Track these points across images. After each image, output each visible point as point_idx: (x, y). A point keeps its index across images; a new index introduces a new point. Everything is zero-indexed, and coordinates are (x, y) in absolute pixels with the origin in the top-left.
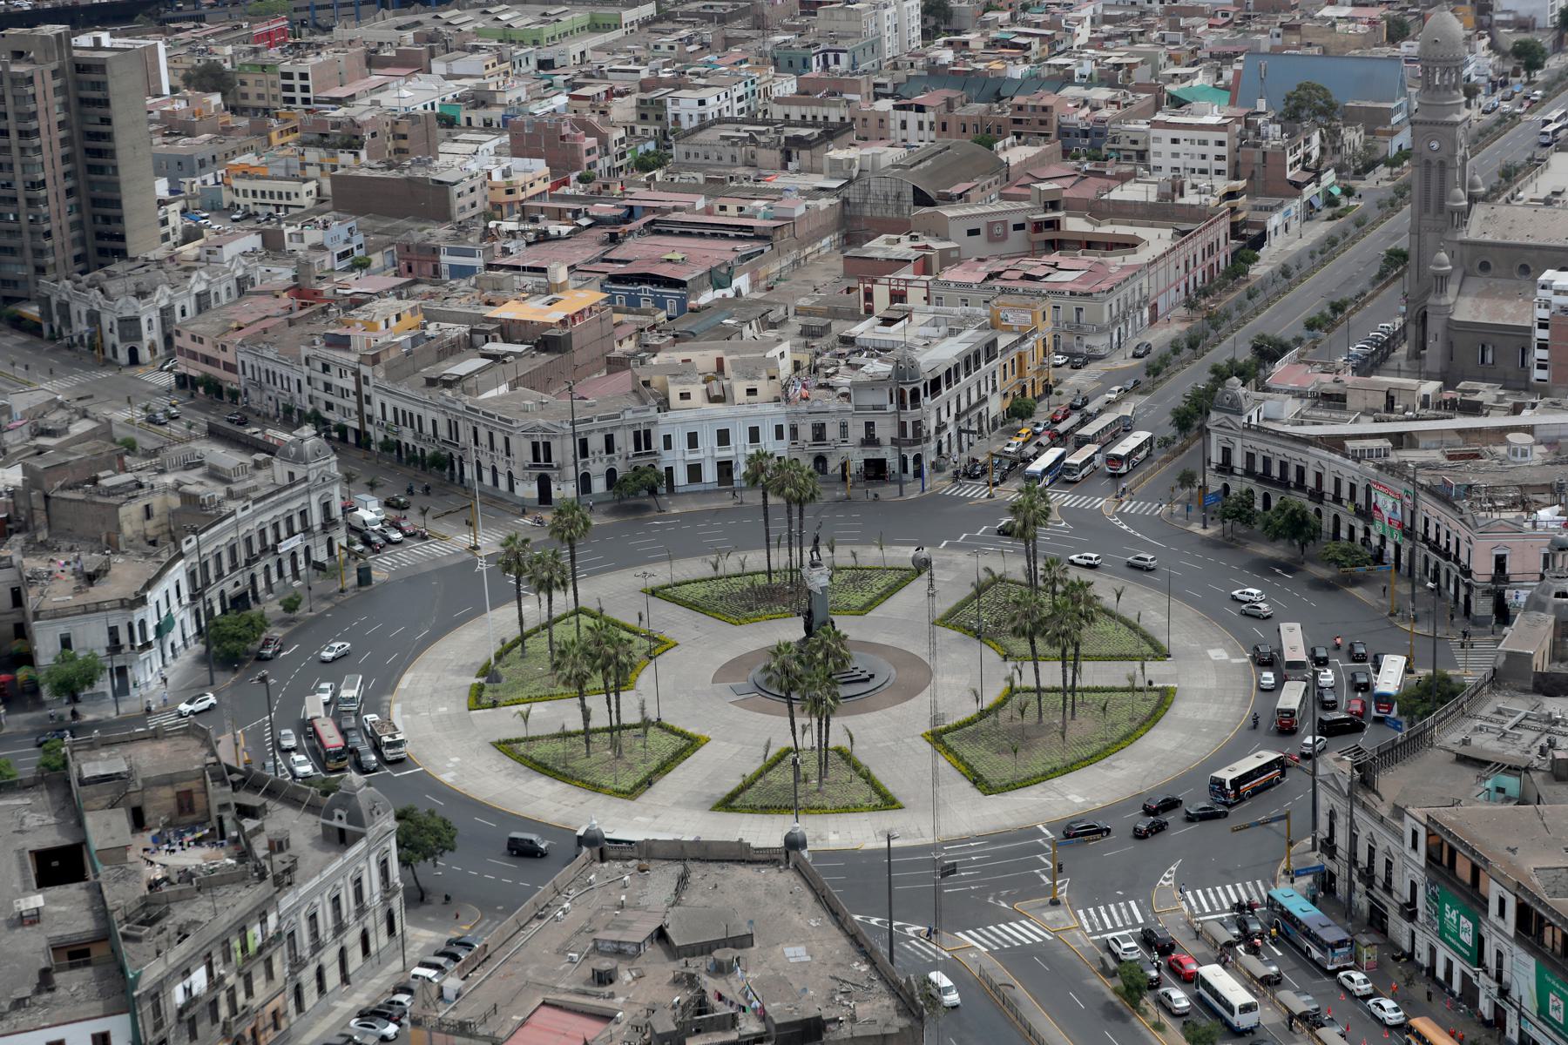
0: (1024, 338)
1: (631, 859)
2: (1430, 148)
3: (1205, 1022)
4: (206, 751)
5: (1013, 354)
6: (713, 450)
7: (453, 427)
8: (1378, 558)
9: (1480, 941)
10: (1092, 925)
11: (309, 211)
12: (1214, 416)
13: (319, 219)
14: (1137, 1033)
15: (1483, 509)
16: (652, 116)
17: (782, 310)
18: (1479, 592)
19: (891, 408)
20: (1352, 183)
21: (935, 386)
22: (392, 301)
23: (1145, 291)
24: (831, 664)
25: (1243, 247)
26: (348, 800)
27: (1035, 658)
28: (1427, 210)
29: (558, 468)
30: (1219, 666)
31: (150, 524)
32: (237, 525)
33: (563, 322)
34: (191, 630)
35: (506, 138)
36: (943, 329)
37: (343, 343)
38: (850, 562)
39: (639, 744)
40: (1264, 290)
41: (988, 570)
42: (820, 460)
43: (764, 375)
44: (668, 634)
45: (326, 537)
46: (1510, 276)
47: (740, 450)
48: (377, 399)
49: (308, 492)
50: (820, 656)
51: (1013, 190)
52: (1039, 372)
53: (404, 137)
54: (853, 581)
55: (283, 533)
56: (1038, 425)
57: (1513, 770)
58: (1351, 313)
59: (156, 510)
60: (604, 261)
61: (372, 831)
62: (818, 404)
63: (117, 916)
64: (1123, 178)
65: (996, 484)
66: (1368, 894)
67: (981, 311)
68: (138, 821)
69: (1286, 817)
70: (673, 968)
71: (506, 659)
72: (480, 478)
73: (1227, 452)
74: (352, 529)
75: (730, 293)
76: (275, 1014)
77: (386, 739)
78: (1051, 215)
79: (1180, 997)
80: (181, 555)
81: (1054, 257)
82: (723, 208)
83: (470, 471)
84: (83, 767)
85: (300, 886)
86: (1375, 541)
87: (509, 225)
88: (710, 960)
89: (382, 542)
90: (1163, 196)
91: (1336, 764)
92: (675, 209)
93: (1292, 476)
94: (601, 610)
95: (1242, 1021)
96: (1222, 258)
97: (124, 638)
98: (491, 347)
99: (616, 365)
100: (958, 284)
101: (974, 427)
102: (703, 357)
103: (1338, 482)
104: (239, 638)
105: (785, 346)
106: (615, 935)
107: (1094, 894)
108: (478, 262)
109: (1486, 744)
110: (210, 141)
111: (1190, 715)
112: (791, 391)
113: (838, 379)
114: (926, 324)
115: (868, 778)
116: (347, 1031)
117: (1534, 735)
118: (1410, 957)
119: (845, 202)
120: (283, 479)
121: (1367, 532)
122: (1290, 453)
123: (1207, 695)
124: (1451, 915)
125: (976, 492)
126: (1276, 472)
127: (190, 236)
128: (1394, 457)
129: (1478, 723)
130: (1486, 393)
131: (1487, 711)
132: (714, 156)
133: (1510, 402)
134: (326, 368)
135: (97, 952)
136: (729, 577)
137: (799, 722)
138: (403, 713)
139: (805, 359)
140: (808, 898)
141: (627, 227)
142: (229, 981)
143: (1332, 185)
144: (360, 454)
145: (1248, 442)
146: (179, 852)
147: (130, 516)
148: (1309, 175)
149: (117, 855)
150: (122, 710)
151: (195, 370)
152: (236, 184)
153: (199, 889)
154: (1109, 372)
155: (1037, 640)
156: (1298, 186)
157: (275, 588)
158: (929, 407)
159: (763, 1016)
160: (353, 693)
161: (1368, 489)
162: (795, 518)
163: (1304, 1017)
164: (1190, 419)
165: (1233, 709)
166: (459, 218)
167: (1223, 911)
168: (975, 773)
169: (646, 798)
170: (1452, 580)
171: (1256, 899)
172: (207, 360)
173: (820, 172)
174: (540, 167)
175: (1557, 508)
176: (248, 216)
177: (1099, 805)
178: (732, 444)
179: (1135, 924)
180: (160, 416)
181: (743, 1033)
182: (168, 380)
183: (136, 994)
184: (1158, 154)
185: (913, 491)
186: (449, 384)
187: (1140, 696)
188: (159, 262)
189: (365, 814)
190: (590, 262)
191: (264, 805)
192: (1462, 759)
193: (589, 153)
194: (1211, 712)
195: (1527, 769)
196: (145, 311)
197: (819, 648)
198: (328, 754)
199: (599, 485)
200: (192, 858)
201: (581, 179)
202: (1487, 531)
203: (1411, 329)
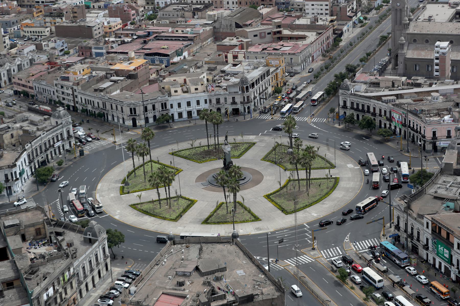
0: (277, 69)
1: (183, 244)
2: (397, 5)
3: (366, 286)
4: (43, 215)
5: (274, 74)
6: (186, 108)
7: (104, 104)
8: (394, 133)
9: (451, 256)
10: (326, 256)
11: (48, 37)
12: (340, 91)
13: (52, 39)
14: (346, 291)
15: (427, 117)
16: (150, 3)
17: (201, 63)
18: (428, 143)
19: (240, 92)
20: (366, 15)
21: (253, 85)
22: (79, 65)
23: (310, 52)
24: (237, 176)
25: (337, 37)
26: (91, 229)
27: (297, 169)
28: (396, 24)
29: (138, 116)
30: (351, 169)
31: (13, 140)
32: (41, 139)
33: (134, 70)
34: (29, 173)
35: (107, 11)
36: (252, 67)
37: (67, 79)
38: (233, 141)
39: (176, 203)
40: (345, 50)
41: (277, 142)
42: (219, 109)
43: (200, 84)
44: (179, 167)
45: (69, 141)
46: (423, 44)
47: (194, 108)
48: (79, 97)
49: (62, 127)
50: (233, 174)
51: (265, 22)
52: (282, 79)
53: (76, 13)
54: (234, 147)
55: (56, 141)
56: (283, 95)
57: (452, 200)
58: (372, 56)
59: (15, 135)
60: (143, 49)
61: (100, 239)
62: (217, 92)
63: (22, 272)
64: (298, 17)
65: (273, 115)
66: (411, 242)
67: (262, 60)
68: (24, 238)
69: (383, 218)
70: (203, 279)
71: (130, 177)
72: (114, 120)
73: (345, 102)
74: (76, 138)
75: (182, 57)
76: (74, 299)
77: (96, 206)
78: (278, 30)
79: (358, 278)
80: (25, 150)
81: (281, 43)
82: (177, 31)
83: (110, 118)
84: (5, 222)
85: (79, 258)
86: (393, 128)
87: (112, 39)
88: (214, 276)
89: (85, 142)
90: (312, 22)
91: (397, 201)
92: (163, 32)
93: (366, 108)
94: (158, 161)
95: (379, 285)
96: (331, 40)
97: (10, 177)
98: (113, 78)
99: (152, 82)
100: (254, 52)
101: (265, 97)
102: (180, 79)
103: (380, 110)
104: (45, 175)
105: (205, 74)
106: (183, 270)
107: (325, 246)
108: (104, 51)
109: (442, 192)
110: (15, 16)
111: (345, 186)
112: (208, 88)
113: (222, 84)
114: (246, 66)
115: (249, 211)
116: (97, 303)
117: (457, 189)
118: (427, 261)
119: (214, 28)
120: (54, 124)
121: (390, 125)
122: (365, 102)
123: (349, 179)
124: (441, 248)
125: (267, 117)
126: (360, 108)
127: (13, 46)
128: (397, 102)
129: (439, 186)
130: (421, 80)
131: (440, 181)
132: (171, 15)
133: (428, 82)
134: (62, 87)
135: (16, 283)
136: (195, 148)
137: (227, 194)
138: (100, 197)
139: (210, 78)
140: (241, 254)
141: (149, 38)
142: (60, 291)
143: (360, 17)
144: (74, 113)
145: (351, 99)
146: (38, 248)
147: (7, 137)
148: (354, 14)
149: (18, 251)
150: (10, 200)
151: (20, 89)
152: (25, 29)
153: (47, 261)
154: (302, 77)
155: (298, 165)
156: (351, 17)
157: (54, 158)
158: (251, 92)
159: (234, 294)
160: (84, 191)
161: (390, 112)
162: (216, 127)
163: (398, 283)
164: (332, 91)
165: (358, 183)
166: (95, 37)
167: (366, 249)
168: (282, 208)
169: (181, 221)
170: (419, 139)
171: (376, 245)
172: (24, 86)
173: (205, 18)
174: (119, 20)
175: (450, 116)
176: (29, 39)
177: (322, 216)
178: (192, 106)
179: (340, 255)
180: (10, 104)
181: (229, 301)
182: (12, 92)
183: (32, 298)
184: (308, 9)
185: (248, 118)
186: (101, 91)
187: (329, 180)
188: (5, 55)
189: (97, 233)
190: (139, 50)
191: (64, 232)
192: (436, 198)
193: (133, 15)
194: (351, 184)
195: (456, 200)
196: (2, 71)
197: (232, 172)
198: (79, 212)
199: (151, 120)
200: (42, 250)
201: (132, 24)
202: (430, 123)
203: (393, 61)
